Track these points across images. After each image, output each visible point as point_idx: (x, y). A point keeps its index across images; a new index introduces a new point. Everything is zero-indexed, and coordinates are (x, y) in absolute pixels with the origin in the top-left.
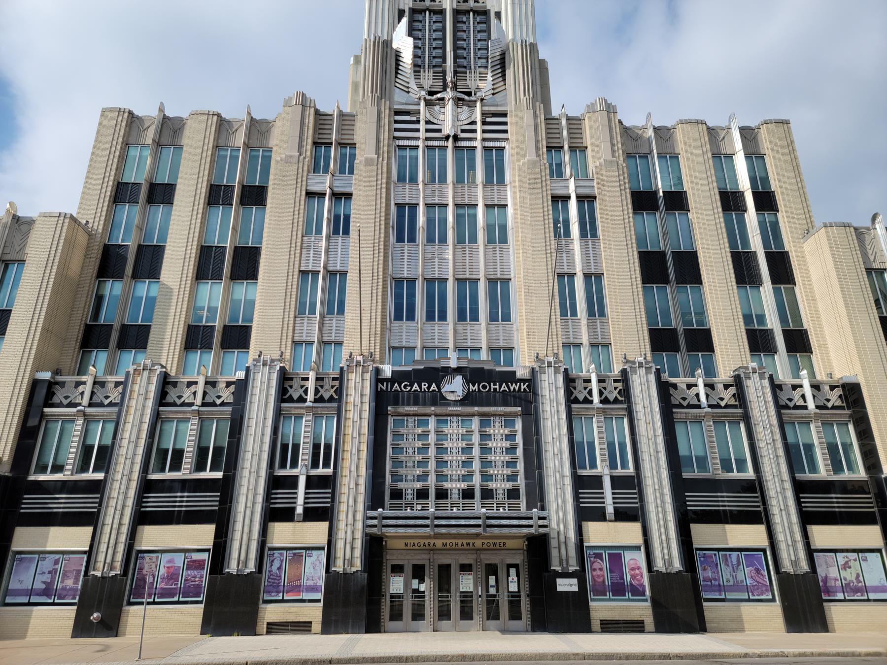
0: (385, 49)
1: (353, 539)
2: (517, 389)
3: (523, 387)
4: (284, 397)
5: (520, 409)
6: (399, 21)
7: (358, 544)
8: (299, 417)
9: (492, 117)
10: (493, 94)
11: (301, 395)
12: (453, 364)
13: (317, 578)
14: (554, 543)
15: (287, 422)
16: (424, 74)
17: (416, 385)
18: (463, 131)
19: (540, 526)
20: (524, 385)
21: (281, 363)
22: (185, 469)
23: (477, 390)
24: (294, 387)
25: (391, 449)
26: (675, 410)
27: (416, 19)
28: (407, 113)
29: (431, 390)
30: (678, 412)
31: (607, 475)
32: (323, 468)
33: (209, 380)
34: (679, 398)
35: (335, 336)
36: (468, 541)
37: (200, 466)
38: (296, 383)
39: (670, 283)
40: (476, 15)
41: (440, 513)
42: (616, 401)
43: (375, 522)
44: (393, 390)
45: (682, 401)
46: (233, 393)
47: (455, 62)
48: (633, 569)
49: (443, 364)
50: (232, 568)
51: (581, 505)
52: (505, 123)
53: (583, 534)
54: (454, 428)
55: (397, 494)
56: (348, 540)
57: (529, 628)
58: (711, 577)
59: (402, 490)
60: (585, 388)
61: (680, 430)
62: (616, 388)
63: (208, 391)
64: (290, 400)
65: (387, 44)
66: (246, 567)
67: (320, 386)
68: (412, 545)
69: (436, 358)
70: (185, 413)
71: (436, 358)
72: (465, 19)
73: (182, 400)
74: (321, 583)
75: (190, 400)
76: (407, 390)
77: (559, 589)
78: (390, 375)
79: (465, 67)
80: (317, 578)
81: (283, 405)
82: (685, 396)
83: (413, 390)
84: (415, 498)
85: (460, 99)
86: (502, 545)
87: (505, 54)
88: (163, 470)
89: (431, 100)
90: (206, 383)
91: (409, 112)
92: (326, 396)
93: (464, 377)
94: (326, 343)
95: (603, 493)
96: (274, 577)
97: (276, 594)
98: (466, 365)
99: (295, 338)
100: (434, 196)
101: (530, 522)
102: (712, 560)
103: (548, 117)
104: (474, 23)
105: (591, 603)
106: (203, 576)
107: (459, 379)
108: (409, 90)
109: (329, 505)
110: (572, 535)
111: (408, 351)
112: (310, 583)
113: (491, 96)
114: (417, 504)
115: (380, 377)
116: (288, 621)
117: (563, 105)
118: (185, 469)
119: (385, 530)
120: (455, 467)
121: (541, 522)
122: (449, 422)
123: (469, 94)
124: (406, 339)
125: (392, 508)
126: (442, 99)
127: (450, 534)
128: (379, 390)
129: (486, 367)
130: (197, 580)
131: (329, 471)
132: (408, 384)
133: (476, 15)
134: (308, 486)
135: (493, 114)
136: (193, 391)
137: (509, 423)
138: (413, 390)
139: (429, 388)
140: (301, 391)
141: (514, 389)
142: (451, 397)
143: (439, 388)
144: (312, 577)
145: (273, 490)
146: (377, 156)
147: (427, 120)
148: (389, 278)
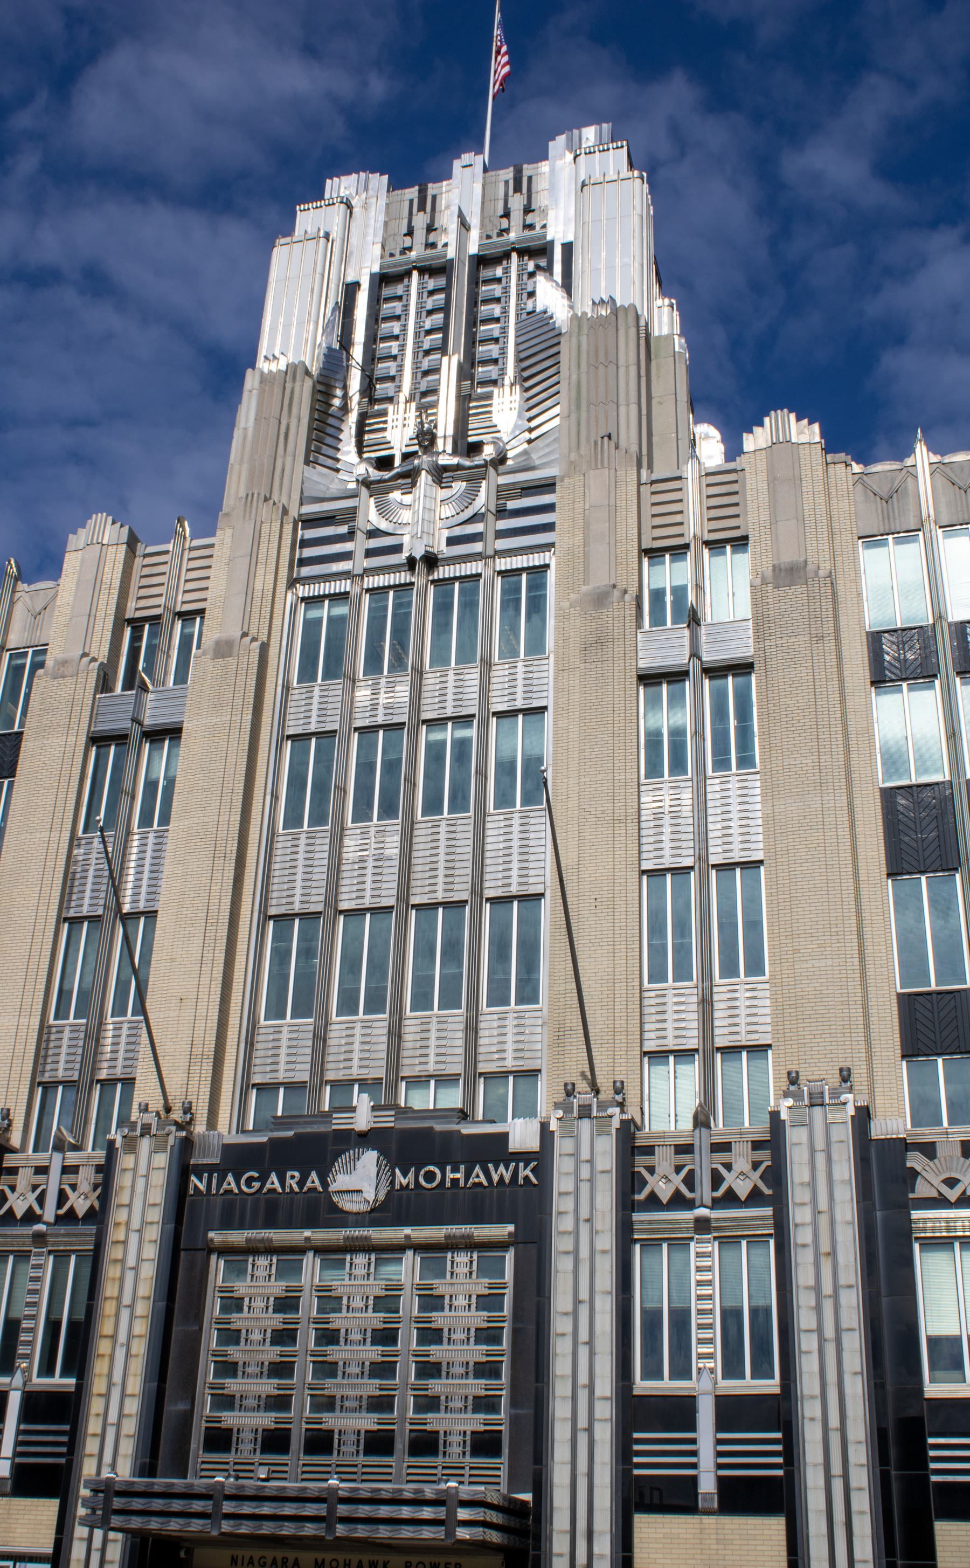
2: (507, 1181)
5: (511, 1228)
8: (680, 1244)
9: (521, 496)
17: (274, 1177)
18: (451, 541)
20: (525, 1168)
23: (412, 1186)
24: (18, 1188)
26: (916, 1214)
29: (305, 1189)
30: (925, 1220)
32: (62, 1376)
34: (936, 1181)
35: (66, 1069)
38: (664, 1160)
44: (222, 1191)
45: (945, 1190)
49: (339, 1122)
51: (636, 1472)
52: (550, 508)
54: (462, 1279)
59: (333, 1431)
60: (35, 1188)
62: (678, 1169)
64: (653, 1202)
76: (253, 1190)
81: (636, 1217)
82: (954, 1175)
83: (265, 1190)
88: (658, 1375)
91: (334, 517)
92: (743, 1189)
93: (382, 1152)
95: (693, 1441)
98: (392, 1125)
107: (370, 1159)
109: (63, 1461)
111: (521, 1081)
113: (525, 446)
114: (261, 1464)
117: (471, 165)
122: (348, 1265)
127: (301, 1538)
131: (771, 1386)
132: (256, 1175)
134: (723, 1422)
137: (492, 1269)
138: (265, 1190)
139: (301, 1183)
140: (32, 1198)
141: (502, 1178)
142: (349, 1205)
143: (325, 1184)
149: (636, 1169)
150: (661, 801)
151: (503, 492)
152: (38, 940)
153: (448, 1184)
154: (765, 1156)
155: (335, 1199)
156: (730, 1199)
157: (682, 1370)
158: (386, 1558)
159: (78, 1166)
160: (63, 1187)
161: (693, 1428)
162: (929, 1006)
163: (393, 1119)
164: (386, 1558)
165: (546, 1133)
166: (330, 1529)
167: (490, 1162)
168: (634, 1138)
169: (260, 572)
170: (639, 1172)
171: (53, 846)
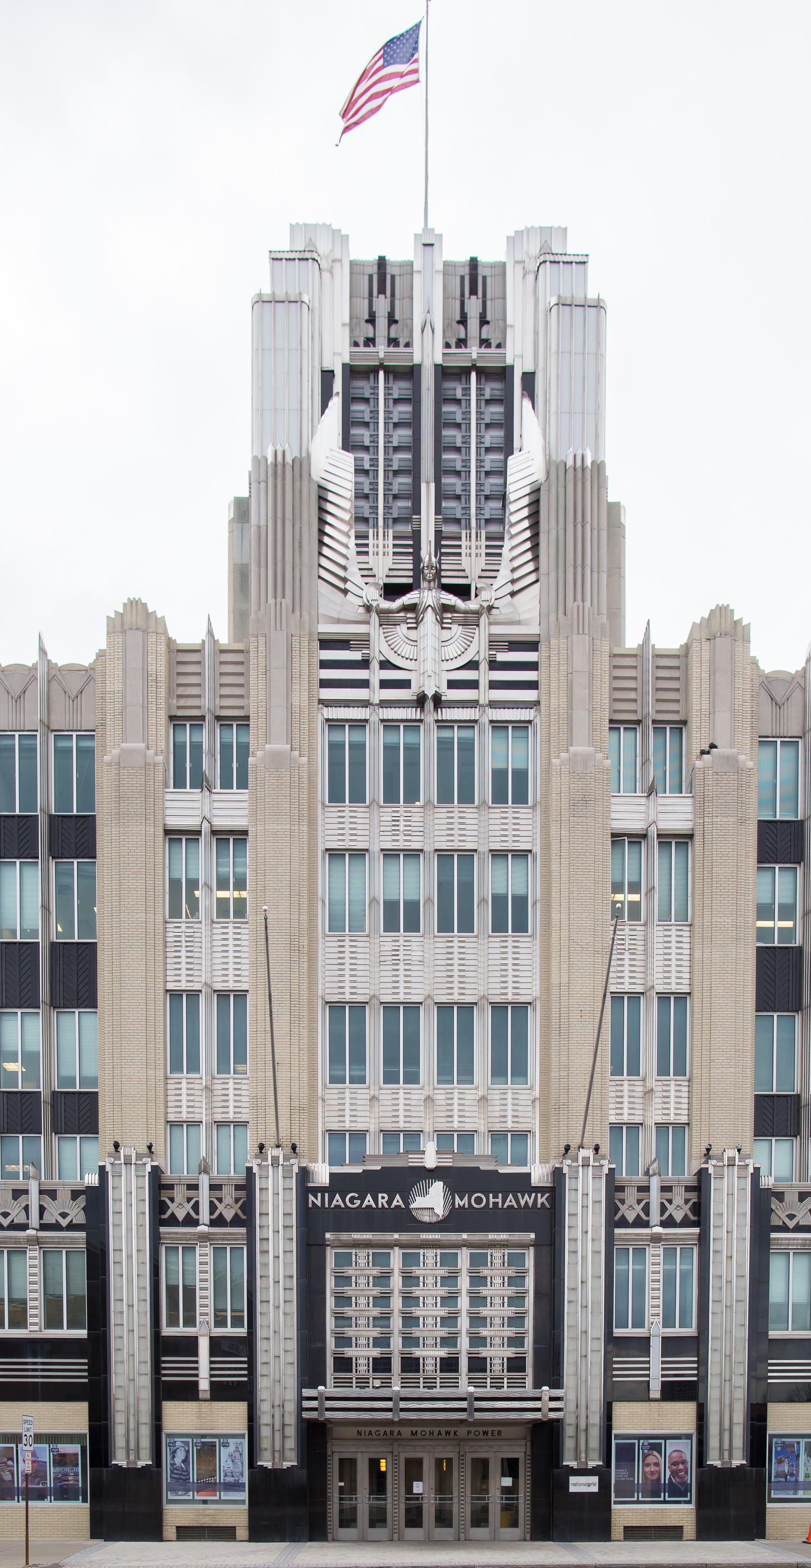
0: (297, 484)
1: (712, 712)
2: (530, 1205)
3: (540, 1201)
4: (163, 1217)
5: (533, 1236)
6: (324, 406)
7: (291, 1431)
8: (189, 1250)
9: (510, 650)
10: (513, 594)
11: (188, 1213)
12: (430, 1160)
13: (238, 1474)
14: (569, 1431)
15: (172, 1259)
16: (376, 542)
17: (369, 1197)
18: (453, 684)
19: (551, 1410)
20: (542, 1197)
21: (152, 1160)
22: (32, 1324)
23: (466, 1206)
25: (333, 1298)
26: (773, 1235)
27: (357, 393)
28: (343, 643)
29: (393, 1206)
30: (778, 1239)
31: (740, 1399)
33: (44, 1188)
34: (783, 1216)
36: (448, 1429)
37: (52, 1321)
38: (180, 1194)
39: (802, 1011)
40: (483, 380)
41: (407, 1392)
42: (685, 1224)
43: (314, 1404)
44: (332, 1206)
46: (84, 1209)
47: (438, 511)
48: (675, 1464)
49: (414, 1161)
50: (120, 1460)
51: (164, 1379)
53: (613, 1418)
55: (344, 1364)
56: (277, 1426)
57: (528, 1536)
58: (786, 1472)
61: (776, 1266)
63: (45, 1205)
64: (173, 1221)
65: (302, 465)
66: (139, 1459)
67: (217, 1199)
68: (367, 1434)
69: (402, 1151)
70: (17, 1240)
71: (402, 1151)
72: (459, 394)
73: (9, 1219)
74: (245, 1480)
75: (21, 1219)
76: (355, 1206)
77: (572, 1489)
78: (328, 1181)
79: (458, 521)
80: (238, 1474)
81: (163, 1229)
83: (364, 1206)
84: (371, 1370)
85: (446, 608)
86: (496, 1434)
87: (538, 490)
89: (389, 611)
90: (41, 1192)
91: (348, 641)
94: (220, 1124)
96: (179, 1472)
97: (184, 1493)
98: (451, 1164)
99: (169, 1115)
100: (395, 832)
101: (537, 1404)
102: (792, 1449)
103: (616, 651)
104: (478, 472)
105: (614, 1506)
106: (77, 1476)
107: (437, 1188)
108: (349, 586)
110: (596, 1419)
112: (230, 1479)
114: (373, 1378)
115: (311, 1185)
116: (203, 1525)
117: (432, 245)
118: (32, 1324)
119: (329, 1415)
120: (430, 1286)
121: (553, 1404)
123: (463, 591)
124: (351, 1116)
125: (338, 1383)
126: (412, 608)
128: (310, 1205)
129: (483, 1167)
130: (70, 1478)
131: (242, 1331)
132: (357, 1195)
133: (483, 380)
135: (511, 643)
136: (23, 1205)
138: (364, 1206)
139: (390, 1202)
143: (407, 1204)
144: (232, 1473)
145: (163, 1356)
146: (289, 746)
147: (382, 658)
148: (320, 1002)
149: (162, 1199)
150: (623, 939)
151: (495, 643)
152: (151, 1006)
153: (491, 1206)
154: (242, 1194)
155: (414, 1213)
156: (668, 1223)
157: (190, 1321)
158: (456, 1429)
159: (221, 1185)
160: (211, 1199)
161: (196, 1355)
162: (771, 1104)
163: (451, 1160)
164: (456, 1429)
165: (102, 1172)
166: (471, 1415)
167: (519, 1192)
168: (160, 1178)
169: (296, 687)
170: (164, 1201)
171: (150, 926)
